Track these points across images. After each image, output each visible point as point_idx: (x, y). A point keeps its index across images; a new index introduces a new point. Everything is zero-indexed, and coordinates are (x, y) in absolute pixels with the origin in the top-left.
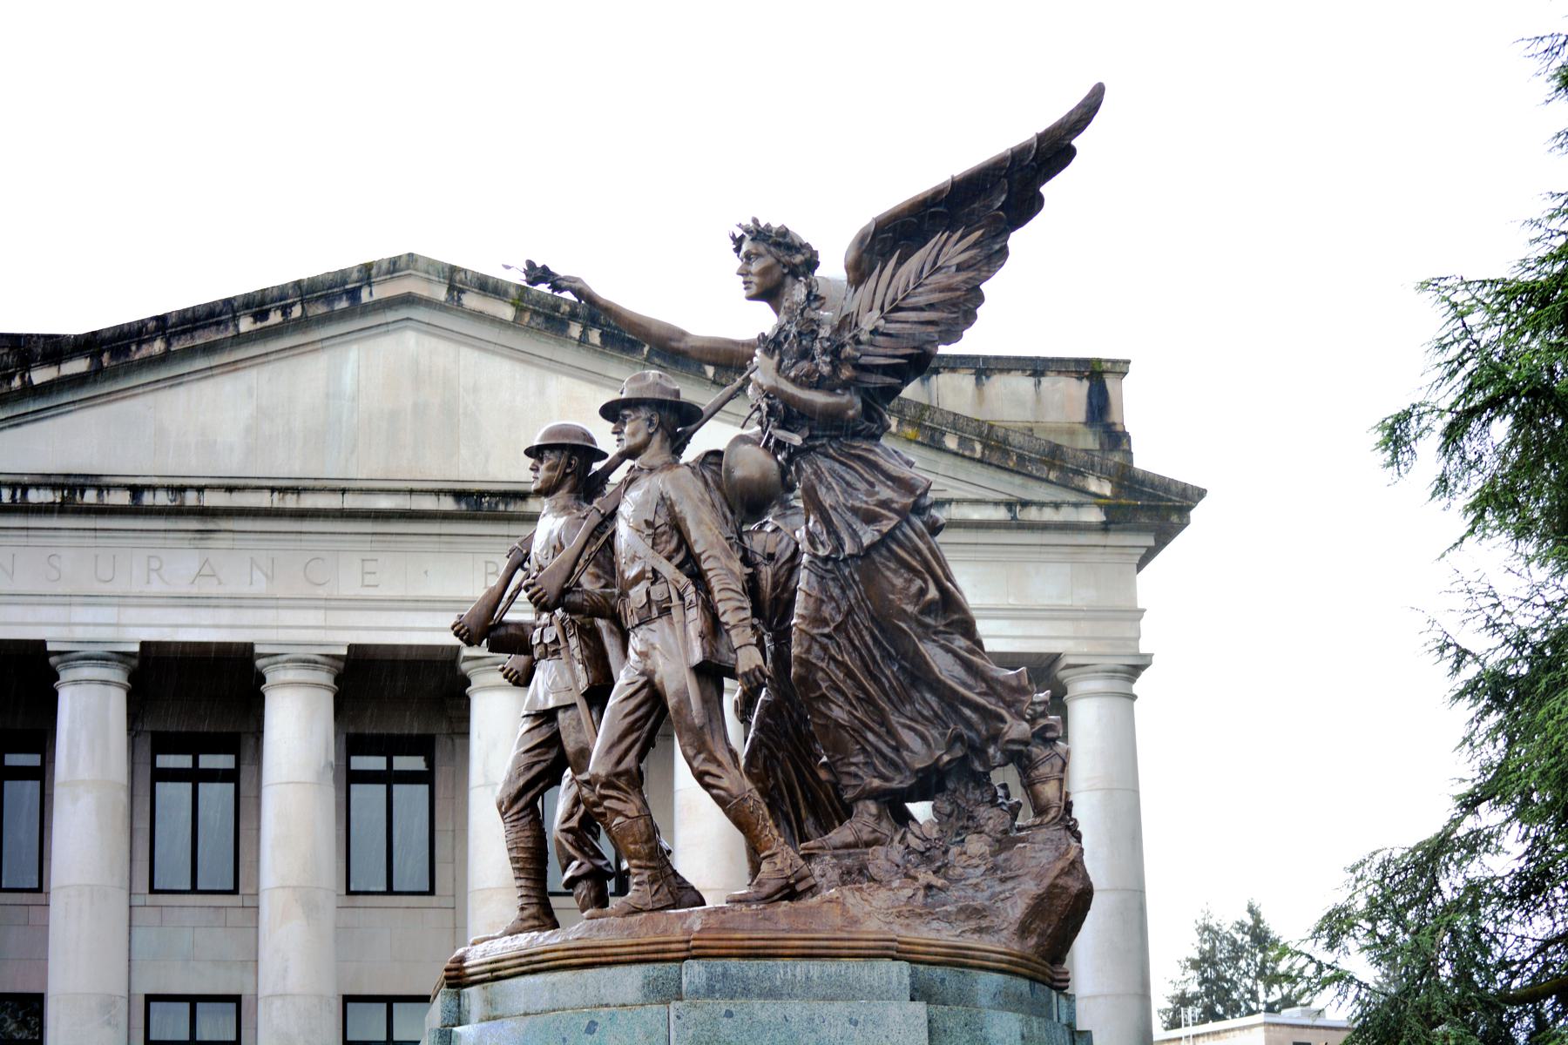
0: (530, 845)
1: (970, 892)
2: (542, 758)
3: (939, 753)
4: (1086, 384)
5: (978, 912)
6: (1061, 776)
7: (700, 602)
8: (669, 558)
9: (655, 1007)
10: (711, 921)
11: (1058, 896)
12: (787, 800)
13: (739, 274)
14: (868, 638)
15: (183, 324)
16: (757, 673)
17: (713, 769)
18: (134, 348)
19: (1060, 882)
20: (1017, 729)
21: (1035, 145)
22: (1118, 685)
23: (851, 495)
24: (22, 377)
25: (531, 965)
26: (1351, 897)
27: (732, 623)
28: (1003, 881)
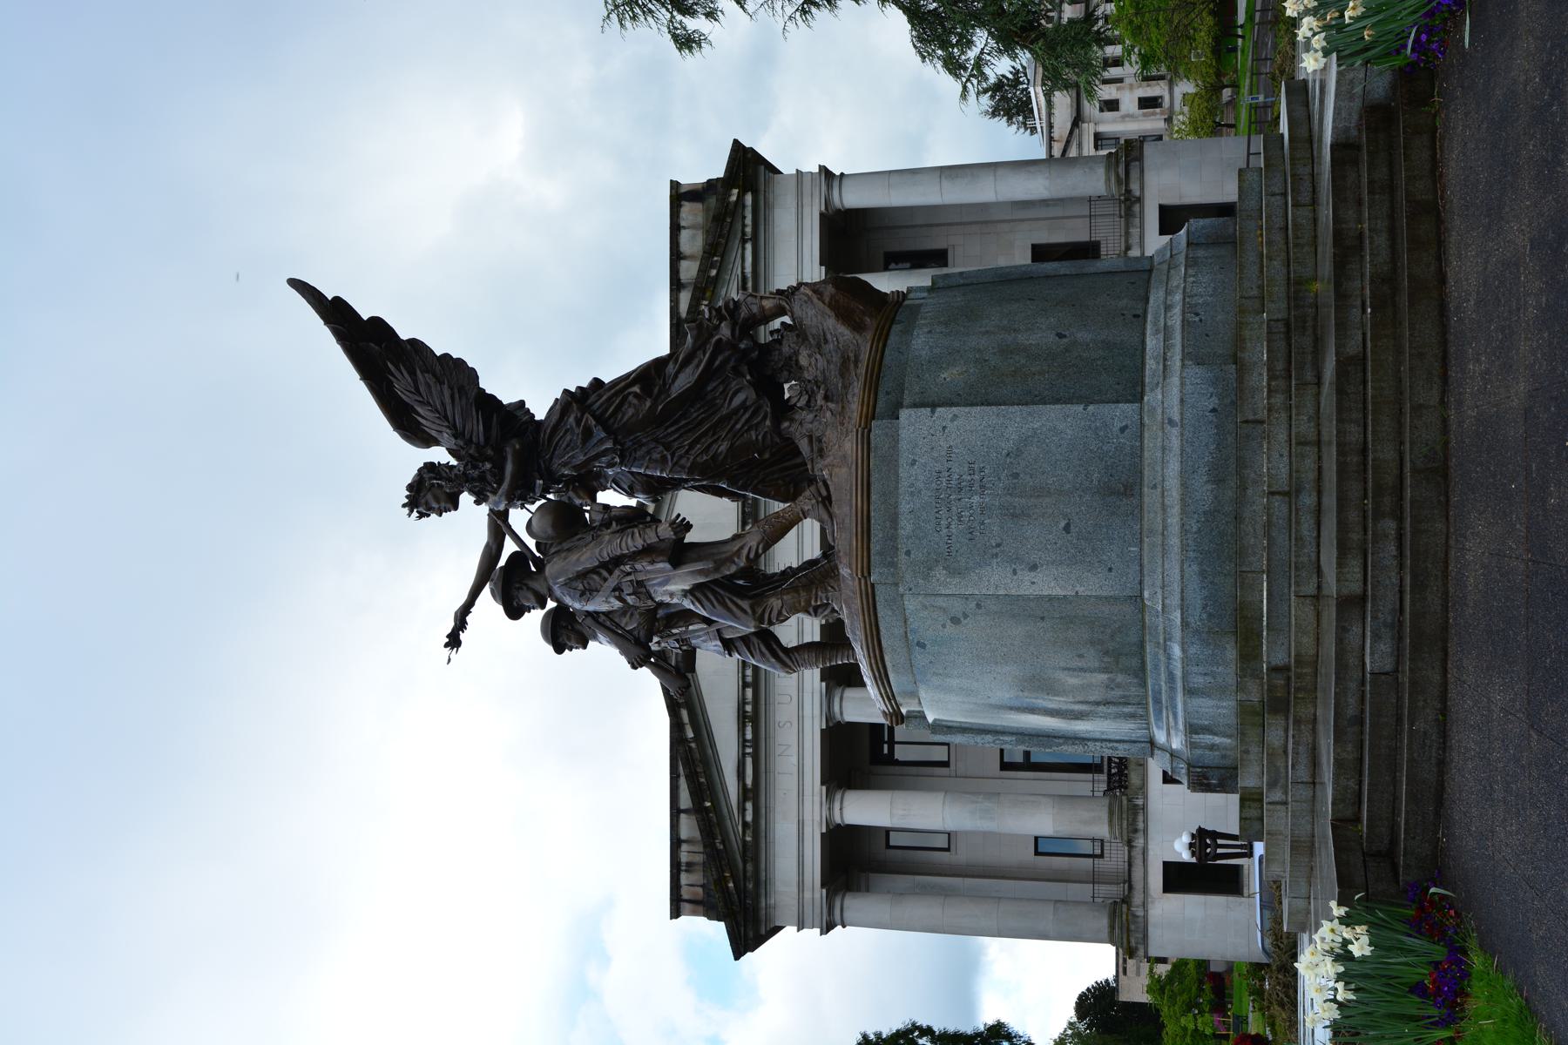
0: (814, 655)
1: (832, 366)
4: (683, 203)
5: (845, 361)
7: (630, 563)
8: (605, 580)
9: (906, 603)
13: (440, 515)
14: (673, 429)
16: (675, 526)
17: (745, 552)
19: (827, 300)
20: (725, 331)
22: (836, 184)
24: (690, 742)
25: (882, 678)
26: (938, 58)
28: (826, 341)
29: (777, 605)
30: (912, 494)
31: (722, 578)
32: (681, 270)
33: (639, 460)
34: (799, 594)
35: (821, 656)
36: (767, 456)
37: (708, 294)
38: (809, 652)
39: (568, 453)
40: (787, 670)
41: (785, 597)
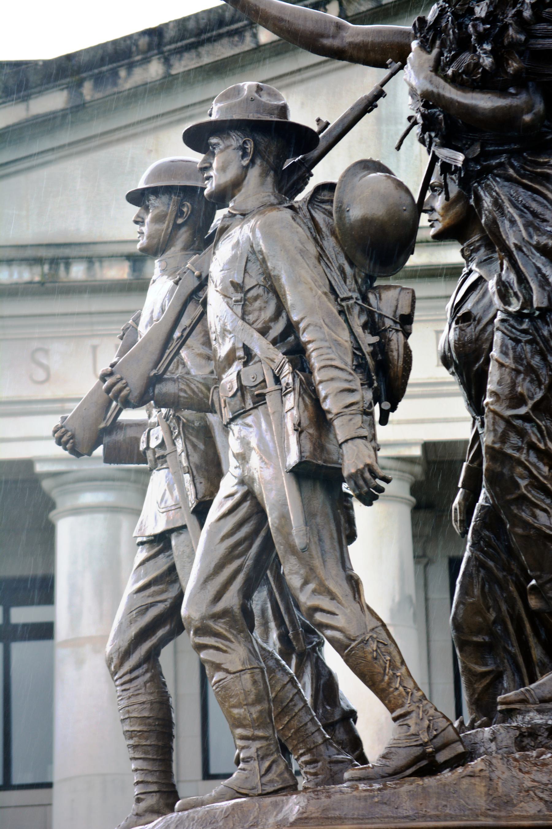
0: (146, 714)
8: (264, 332)
10: (311, 808)
12: (513, 638)
15: (183, 38)
16: (367, 475)
17: (324, 602)
18: (123, 73)
23: (537, 229)
27: (334, 411)
31: (277, 555)
33: (514, 349)
34: (253, 704)
35: (145, 728)
36: (534, 602)
39: (521, 216)
40: (115, 661)
41: (247, 677)
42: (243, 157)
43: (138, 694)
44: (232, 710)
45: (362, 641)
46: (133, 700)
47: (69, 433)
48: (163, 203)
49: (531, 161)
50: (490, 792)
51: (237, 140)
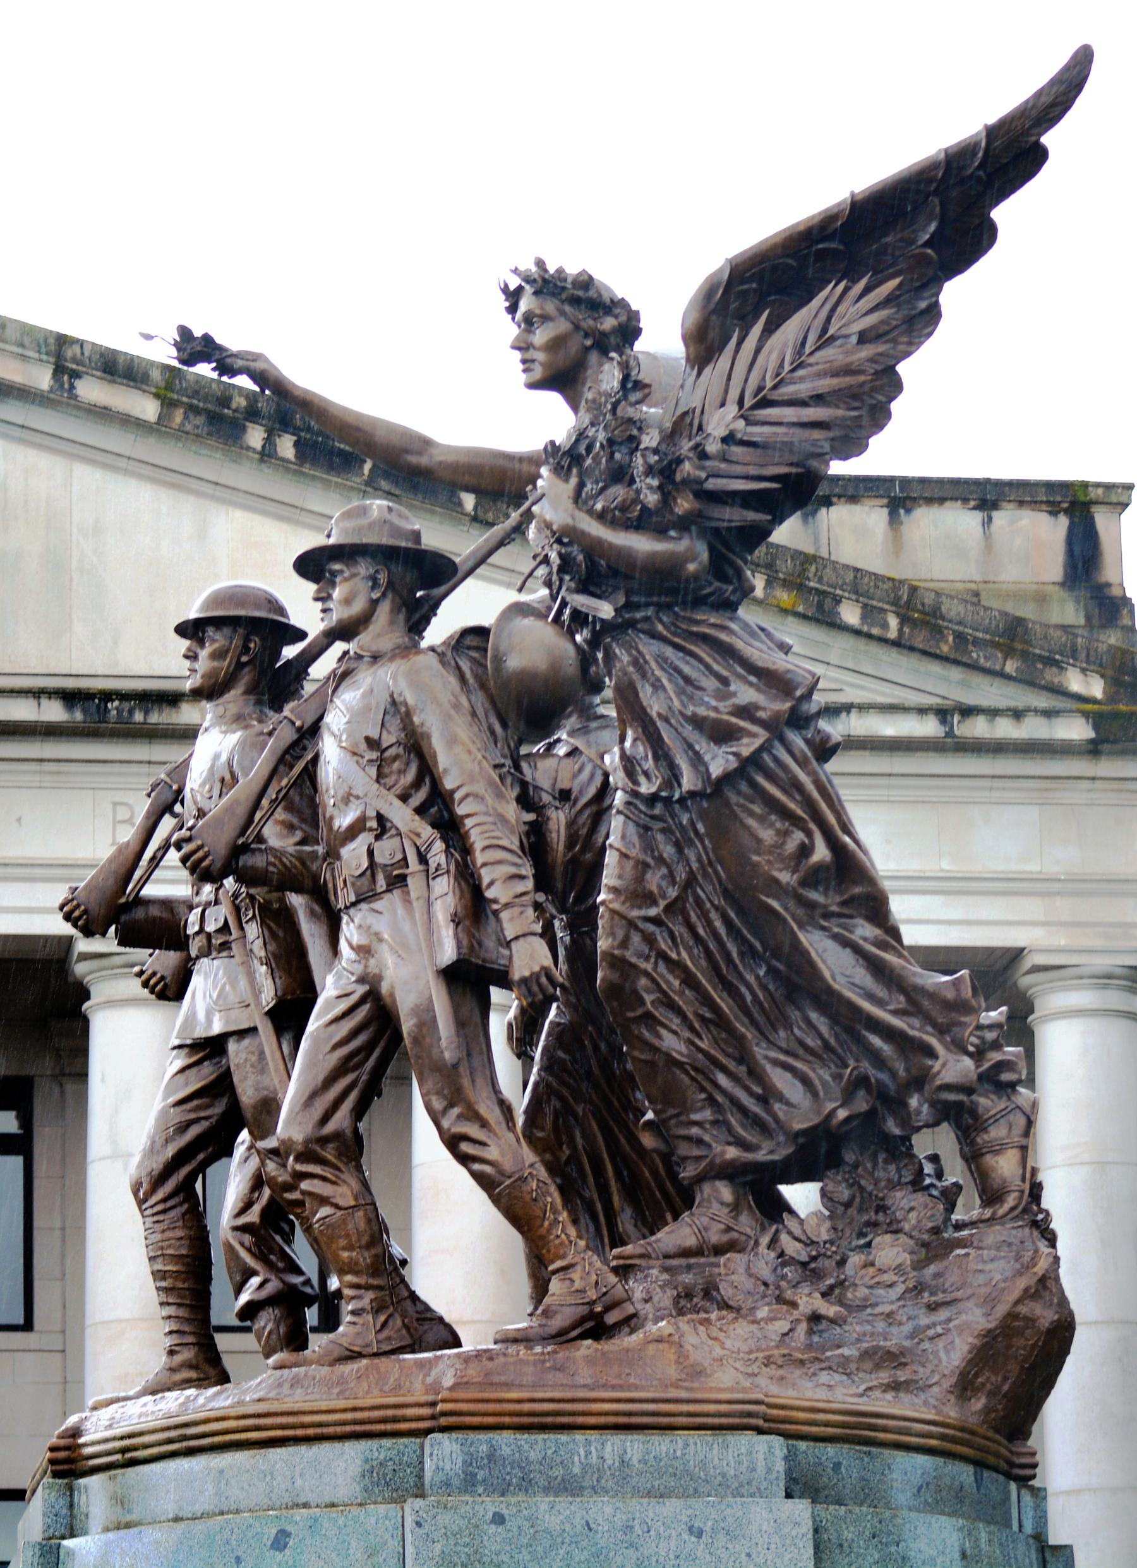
0: (184, 1252)
2: (203, 1114)
3: (830, 1106)
4: (1063, 521)
5: (893, 1358)
6: (1024, 1142)
7: (452, 868)
8: (404, 798)
11: (1020, 1332)
14: (718, 924)
16: (544, 980)
17: (473, 1130)
19: (1023, 1309)
21: (983, 144)
23: (691, 698)
27: (503, 900)
28: (932, 1308)
29: (342, 1196)
30: (628, 1528)
32: (856, 508)
37: (784, 597)
38: (190, 1238)
40: (145, 1186)
42: (373, 588)
43: (175, 1228)
44: (341, 1253)
45: (519, 1179)
46: (169, 1234)
47: (82, 908)
48: (225, 637)
49: (684, 618)
50: (681, 1360)
51: (367, 569)
